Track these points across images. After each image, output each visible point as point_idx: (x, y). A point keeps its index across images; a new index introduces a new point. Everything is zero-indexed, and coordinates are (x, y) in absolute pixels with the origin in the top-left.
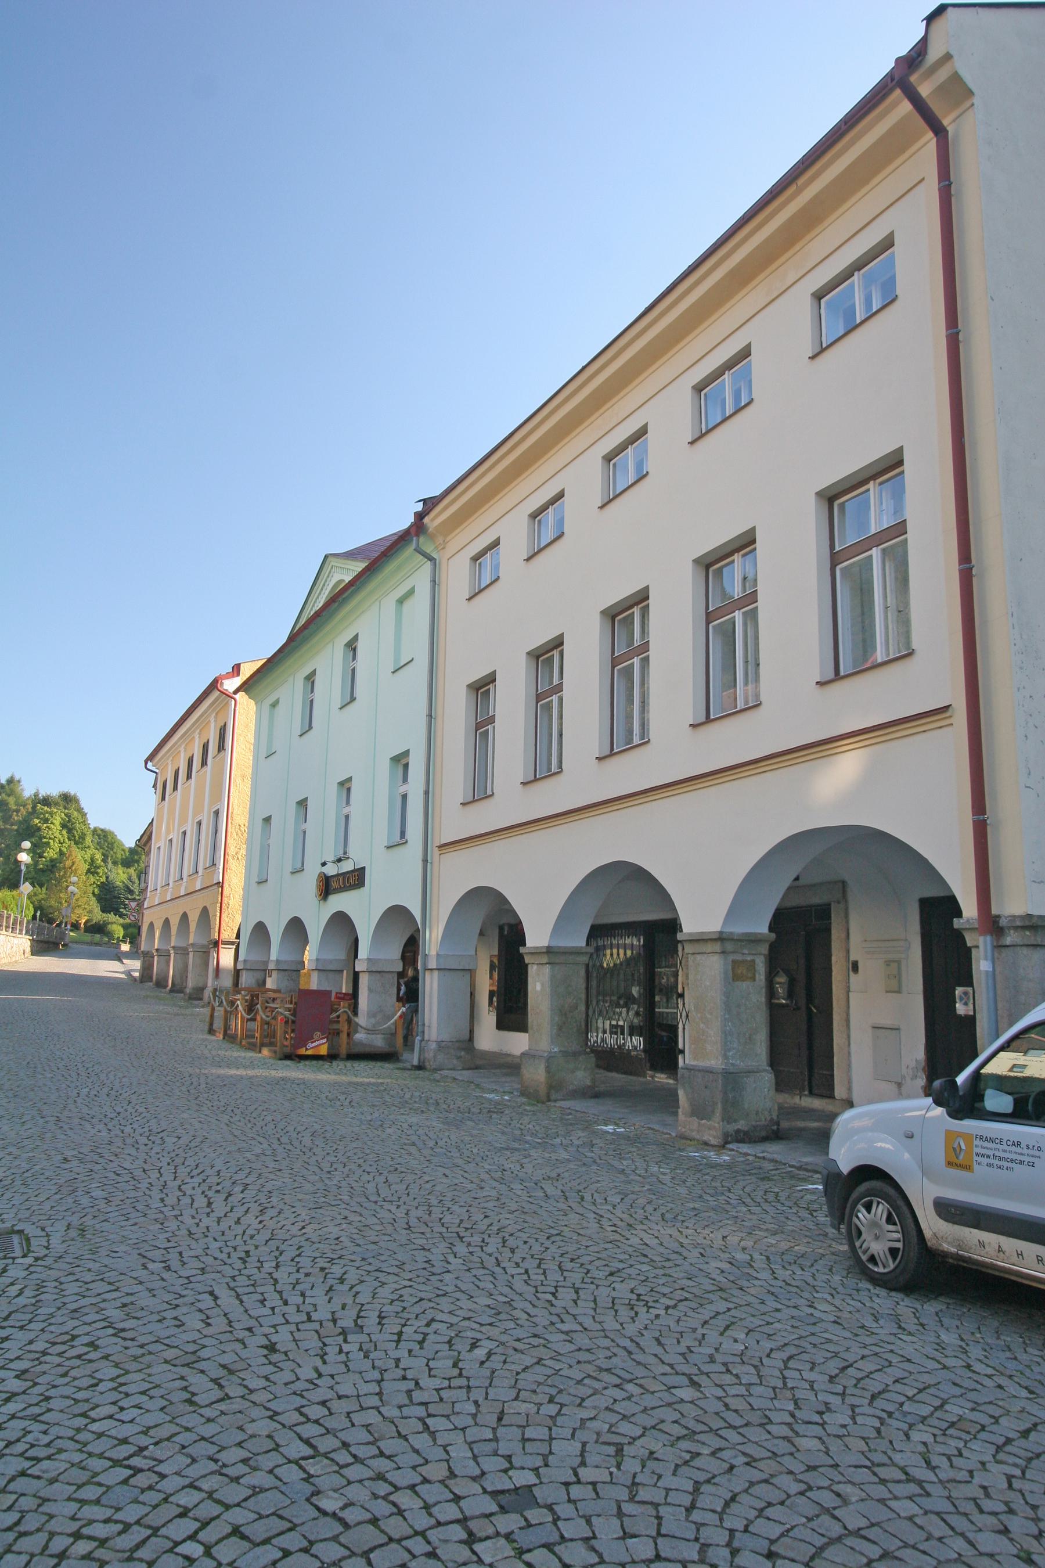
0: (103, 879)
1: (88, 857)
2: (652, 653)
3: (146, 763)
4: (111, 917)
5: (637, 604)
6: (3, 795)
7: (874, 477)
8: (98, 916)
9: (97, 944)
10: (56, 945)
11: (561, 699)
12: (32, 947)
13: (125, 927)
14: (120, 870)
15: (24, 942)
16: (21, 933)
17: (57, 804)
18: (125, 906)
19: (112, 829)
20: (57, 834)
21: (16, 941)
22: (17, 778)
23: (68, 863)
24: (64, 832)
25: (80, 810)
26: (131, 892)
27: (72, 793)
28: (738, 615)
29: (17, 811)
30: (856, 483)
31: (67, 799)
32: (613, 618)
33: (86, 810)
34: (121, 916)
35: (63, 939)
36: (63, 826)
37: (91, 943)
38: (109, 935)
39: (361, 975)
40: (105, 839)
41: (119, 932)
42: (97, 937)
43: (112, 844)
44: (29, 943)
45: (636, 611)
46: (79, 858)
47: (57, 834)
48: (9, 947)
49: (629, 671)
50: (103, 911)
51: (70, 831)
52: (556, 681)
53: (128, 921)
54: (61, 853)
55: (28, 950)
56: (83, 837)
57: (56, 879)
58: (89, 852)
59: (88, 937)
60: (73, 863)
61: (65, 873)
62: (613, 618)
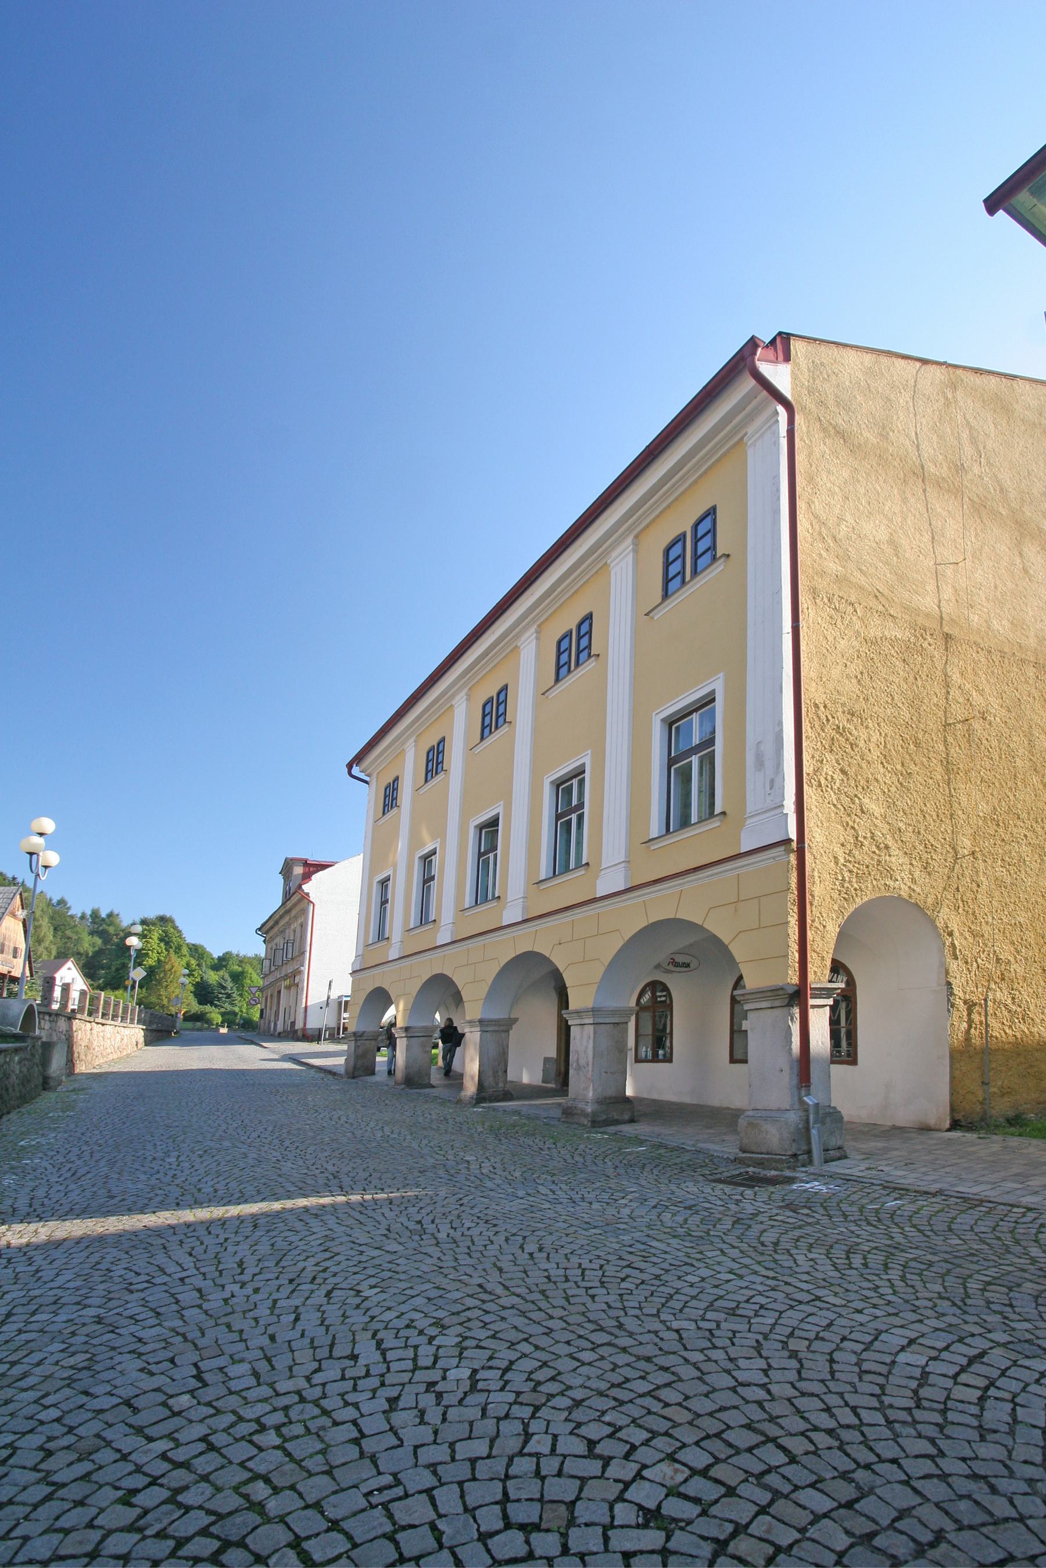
0: (198, 980)
1: (184, 962)
2: (586, 810)
3: (350, 766)
4: (208, 1008)
5: (575, 776)
6: (104, 926)
7: (696, 710)
8: (195, 1007)
9: (199, 1030)
10: (170, 1032)
11: (496, 856)
12: (145, 1036)
13: (223, 1014)
14: (212, 973)
15: (137, 1032)
16: (132, 1021)
17: (154, 924)
18: (219, 999)
19: (202, 943)
20: (155, 946)
21: (127, 1031)
22: (116, 912)
23: (168, 967)
24: (162, 945)
25: (175, 928)
26: (224, 988)
27: (168, 916)
28: (695, 760)
29: (117, 935)
30: (686, 713)
31: (163, 920)
32: (558, 786)
33: (180, 928)
34: (216, 1006)
35: (175, 1027)
36: (161, 940)
37: (193, 1030)
38: (209, 1022)
39: (572, 1028)
40: (197, 951)
41: (218, 1019)
42: (198, 1024)
43: (202, 955)
44: (142, 1033)
45: (575, 782)
46: (178, 965)
47: (155, 946)
48: (118, 1038)
49: (569, 822)
50: (200, 1003)
51: (167, 943)
52: (575, 802)
53: (223, 1010)
54: (159, 960)
55: (141, 1040)
56: (178, 948)
57: (156, 980)
58: (185, 960)
59: (189, 1025)
60: (173, 967)
61: (165, 974)
62: (558, 786)
